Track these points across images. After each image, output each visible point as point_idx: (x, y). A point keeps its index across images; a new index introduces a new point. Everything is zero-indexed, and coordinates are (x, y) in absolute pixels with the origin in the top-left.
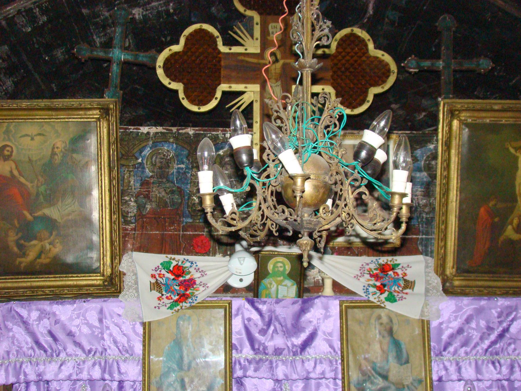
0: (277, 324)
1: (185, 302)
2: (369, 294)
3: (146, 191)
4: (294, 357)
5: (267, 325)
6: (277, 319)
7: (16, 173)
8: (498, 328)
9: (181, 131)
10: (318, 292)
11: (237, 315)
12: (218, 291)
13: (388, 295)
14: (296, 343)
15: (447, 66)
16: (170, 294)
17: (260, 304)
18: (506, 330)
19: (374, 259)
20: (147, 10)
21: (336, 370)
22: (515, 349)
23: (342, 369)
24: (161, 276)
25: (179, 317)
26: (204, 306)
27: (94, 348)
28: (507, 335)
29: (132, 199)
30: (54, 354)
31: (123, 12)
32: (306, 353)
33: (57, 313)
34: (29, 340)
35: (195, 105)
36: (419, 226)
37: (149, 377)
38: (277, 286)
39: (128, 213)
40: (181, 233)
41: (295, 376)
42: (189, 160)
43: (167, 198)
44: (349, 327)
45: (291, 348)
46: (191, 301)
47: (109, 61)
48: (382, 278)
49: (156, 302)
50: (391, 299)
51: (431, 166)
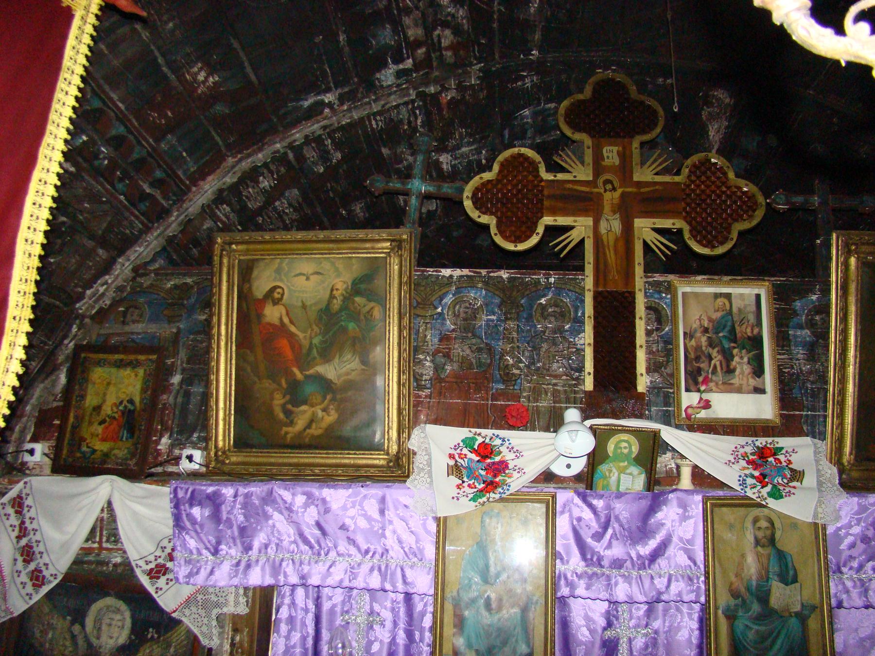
0: (616, 525)
1: (493, 492)
2: (746, 487)
3: (447, 348)
5: (602, 528)
6: (617, 518)
7: (286, 320)
9: (492, 274)
10: (672, 485)
11: (562, 512)
13: (772, 489)
14: (642, 553)
17: (594, 498)
19: (749, 440)
20: (456, 158)
23: (706, 590)
24: (462, 456)
25: (484, 513)
27: (372, 547)
29: (428, 358)
30: (322, 552)
32: (657, 565)
33: (328, 499)
34: (292, 531)
35: (511, 242)
36: (803, 399)
37: (443, 590)
38: (619, 474)
39: (422, 375)
40: (490, 402)
42: (501, 310)
44: (716, 531)
46: (502, 491)
47: (407, 193)
48: (761, 466)
50: (776, 494)
51: (814, 322)
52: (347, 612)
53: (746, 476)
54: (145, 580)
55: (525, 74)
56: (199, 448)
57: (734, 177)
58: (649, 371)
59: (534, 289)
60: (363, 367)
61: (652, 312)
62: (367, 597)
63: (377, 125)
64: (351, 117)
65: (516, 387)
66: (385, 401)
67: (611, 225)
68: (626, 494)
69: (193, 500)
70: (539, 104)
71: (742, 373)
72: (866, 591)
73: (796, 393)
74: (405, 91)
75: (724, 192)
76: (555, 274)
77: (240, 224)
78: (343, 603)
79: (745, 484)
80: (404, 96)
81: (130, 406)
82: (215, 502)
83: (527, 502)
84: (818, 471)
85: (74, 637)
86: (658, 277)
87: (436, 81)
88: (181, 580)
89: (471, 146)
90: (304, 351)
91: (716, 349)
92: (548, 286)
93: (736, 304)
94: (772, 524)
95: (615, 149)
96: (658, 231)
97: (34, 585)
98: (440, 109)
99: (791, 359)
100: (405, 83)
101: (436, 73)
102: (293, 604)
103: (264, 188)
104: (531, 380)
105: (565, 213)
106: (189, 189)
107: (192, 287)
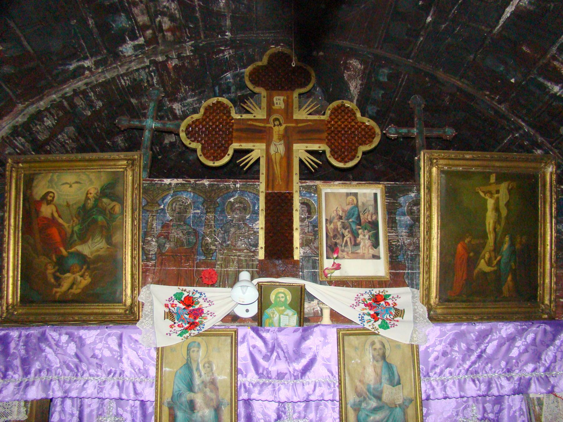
0: (279, 350)
2: (364, 322)
3: (167, 233)
4: (295, 381)
5: (270, 352)
6: (279, 346)
7: (56, 215)
8: (477, 350)
9: (198, 182)
11: (243, 342)
12: (223, 320)
13: (382, 322)
14: (297, 368)
15: (420, 132)
16: (181, 322)
18: (484, 351)
19: (368, 290)
20: (184, 106)
22: (491, 368)
26: (212, 333)
27: (113, 369)
29: (154, 239)
30: (79, 374)
31: (156, 92)
32: (306, 377)
33: (84, 337)
39: (149, 251)
40: (195, 269)
41: (296, 399)
42: (204, 206)
43: (184, 238)
44: (346, 352)
45: (292, 372)
46: (199, 329)
48: (375, 307)
50: (384, 326)
51: (413, 211)
52: (101, 415)
53: (364, 314)
55: (223, 48)
57: (360, 116)
58: (302, 245)
59: (226, 192)
60: (108, 246)
61: (305, 206)
62: (114, 404)
63: (125, 83)
64: (105, 77)
65: (213, 258)
67: (278, 148)
68: (285, 328)
70: (236, 69)
71: (365, 246)
72: (445, 387)
73: (401, 258)
74: (141, 59)
75: (353, 126)
76: (240, 182)
77: (34, 151)
78: (98, 409)
79: (364, 319)
80: (141, 63)
83: (222, 336)
84: (414, 310)
86: (309, 183)
87: (163, 53)
89: (194, 98)
90: (68, 236)
91: (347, 230)
92: (235, 190)
93: (361, 200)
94: (384, 346)
95: (282, 98)
96: (308, 152)
98: (169, 73)
99: (397, 236)
100: (141, 54)
101: (161, 48)
102: (63, 410)
103: (48, 125)
104: (223, 253)
105: (247, 140)
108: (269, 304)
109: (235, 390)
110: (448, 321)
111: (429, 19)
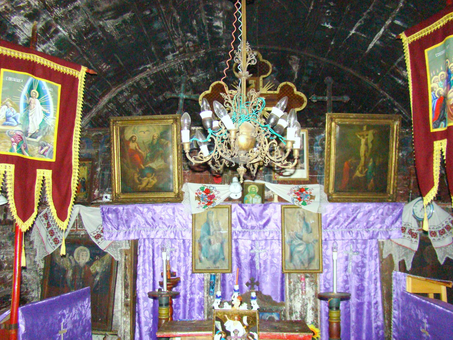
0: (252, 215)
7: (137, 148)
11: (234, 211)
12: (225, 201)
15: (329, 99)
18: (355, 217)
19: (297, 186)
21: (279, 236)
22: (359, 226)
27: (171, 225)
28: (356, 220)
34: (143, 221)
37: (195, 238)
41: (260, 239)
48: (300, 194)
49: (197, 205)
50: (304, 204)
54: (94, 240)
56: (109, 194)
66: (173, 175)
69: (108, 212)
81: (83, 180)
82: (116, 212)
85: (70, 260)
88: (107, 239)
90: (145, 158)
97: (55, 243)
102: (144, 245)
106: (99, 100)
107: (102, 135)
108: (247, 193)
109: (231, 234)
110: (337, 202)
111: (332, 43)
